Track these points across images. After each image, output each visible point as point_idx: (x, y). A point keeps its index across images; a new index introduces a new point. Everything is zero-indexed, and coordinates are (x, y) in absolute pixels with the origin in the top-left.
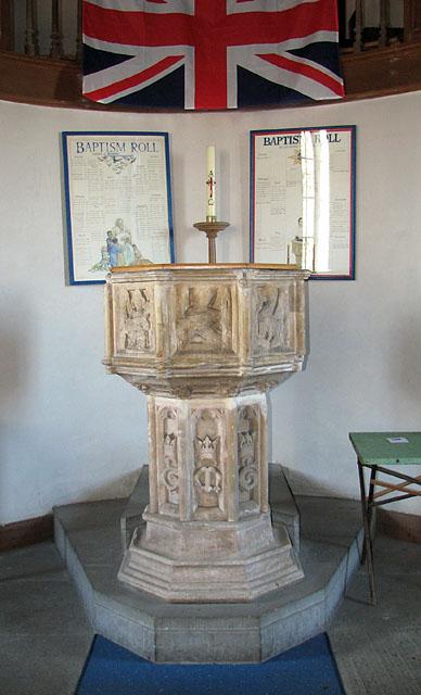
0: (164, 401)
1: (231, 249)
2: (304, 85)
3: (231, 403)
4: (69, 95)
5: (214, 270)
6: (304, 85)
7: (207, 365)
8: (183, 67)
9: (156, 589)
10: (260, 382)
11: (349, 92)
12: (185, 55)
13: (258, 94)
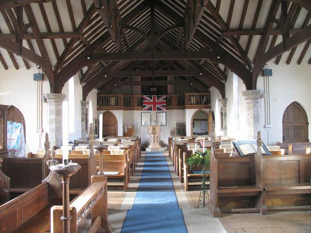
2: (162, 109)
6: (162, 109)
12: (152, 106)
13: (159, 109)
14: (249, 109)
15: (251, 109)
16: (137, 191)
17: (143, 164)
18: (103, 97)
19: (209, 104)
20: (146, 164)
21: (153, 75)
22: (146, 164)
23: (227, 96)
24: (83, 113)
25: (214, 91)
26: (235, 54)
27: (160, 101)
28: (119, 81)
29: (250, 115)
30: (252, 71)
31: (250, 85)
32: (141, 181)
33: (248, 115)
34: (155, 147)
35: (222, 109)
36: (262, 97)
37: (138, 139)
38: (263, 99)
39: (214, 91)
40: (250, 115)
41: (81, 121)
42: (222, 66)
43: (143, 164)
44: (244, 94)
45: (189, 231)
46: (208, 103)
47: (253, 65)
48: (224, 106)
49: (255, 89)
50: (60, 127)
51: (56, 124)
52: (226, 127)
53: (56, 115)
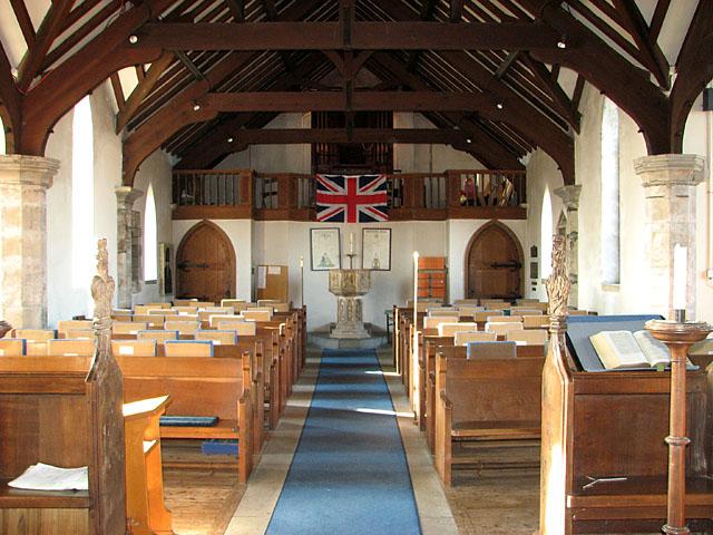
0: (341, 298)
1: (356, 261)
2: (377, 217)
3: (355, 298)
4: (313, 218)
5: (352, 270)
6: (377, 217)
7: (350, 289)
8: (360, 212)
9: (494, 475)
10: (362, 294)
11: (390, 219)
12: (345, 206)
13: (365, 218)
14: (655, 218)
15: (661, 217)
16: (313, 398)
17: (311, 388)
18: (191, 175)
19: (523, 205)
20: (322, 387)
21: (347, 40)
22: (322, 387)
23: (579, 178)
24: (123, 226)
25: (536, 161)
26: (617, 38)
27: (370, 192)
28: (243, 128)
29: (659, 237)
30: (668, 94)
31: (663, 136)
32: (315, 395)
33: (654, 234)
34: (351, 335)
35: (562, 219)
36: (702, 180)
37: (292, 310)
38: (702, 185)
39: (536, 161)
40: (659, 237)
41: (116, 251)
42: (567, 79)
43: (311, 388)
44: (641, 168)
45: (424, 533)
46: (519, 205)
47: (673, 75)
48: (570, 209)
49: (679, 150)
50: (559, 261)
51: (24, 256)
52: (576, 276)
53: (25, 228)
